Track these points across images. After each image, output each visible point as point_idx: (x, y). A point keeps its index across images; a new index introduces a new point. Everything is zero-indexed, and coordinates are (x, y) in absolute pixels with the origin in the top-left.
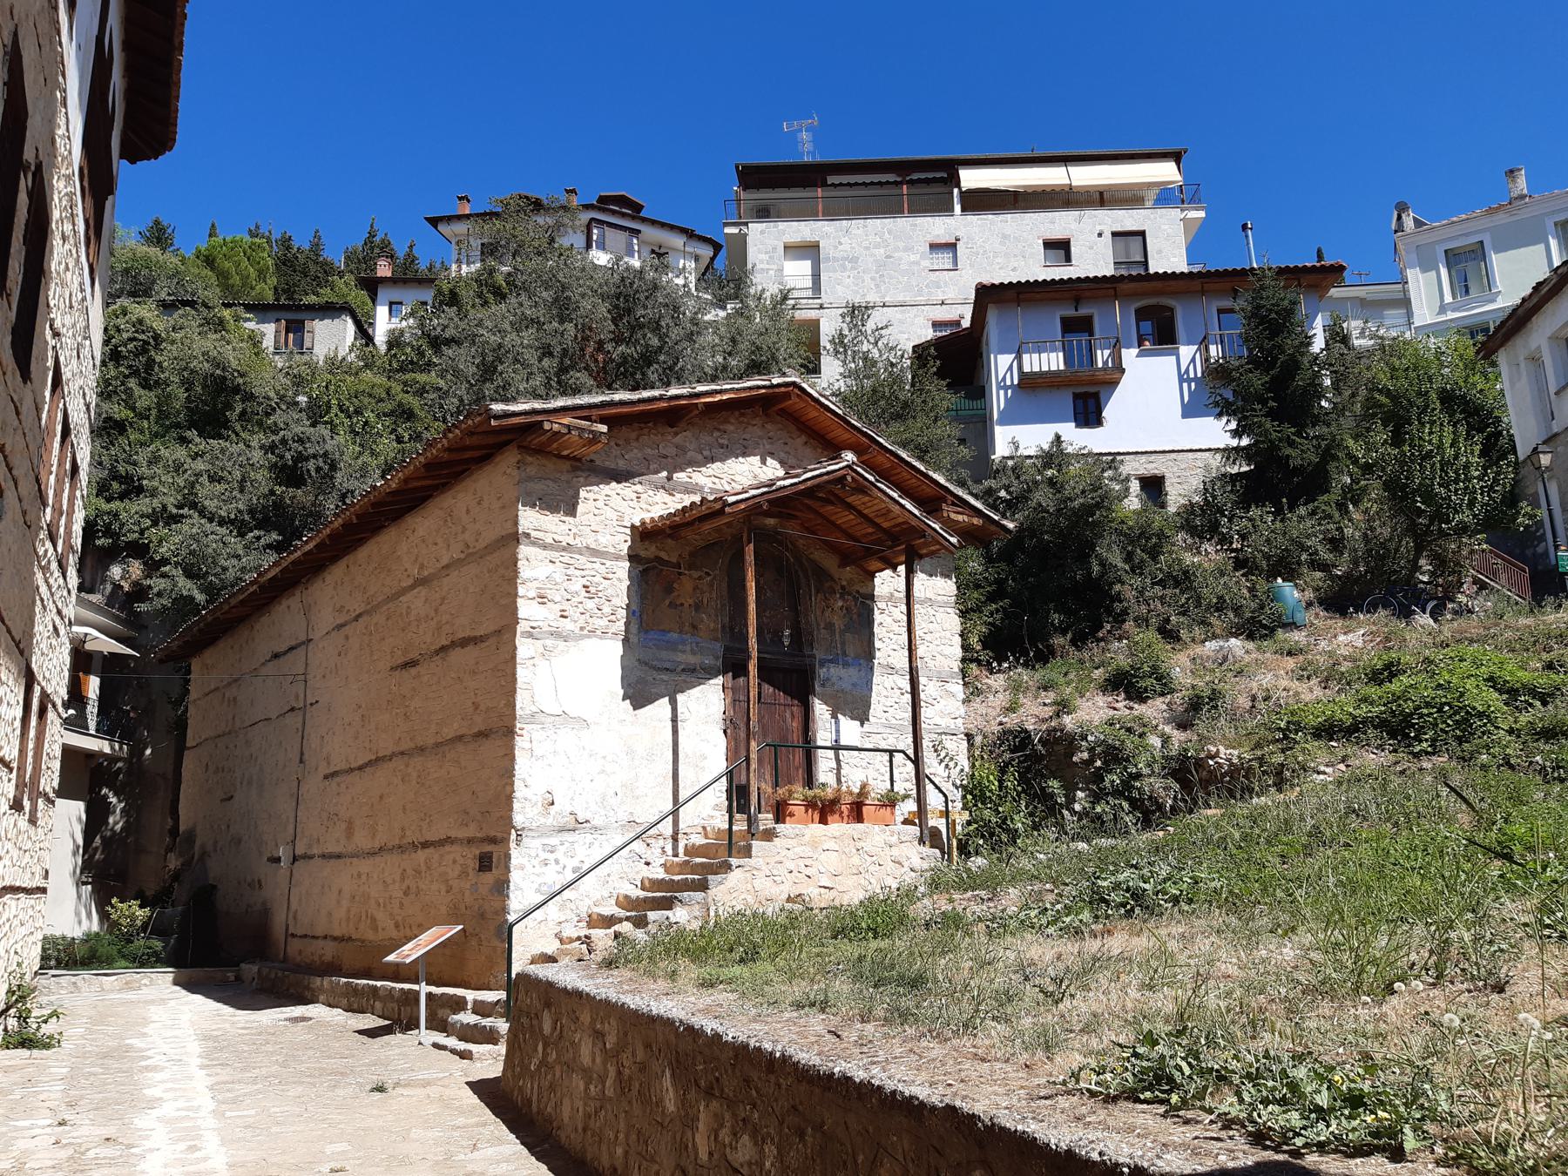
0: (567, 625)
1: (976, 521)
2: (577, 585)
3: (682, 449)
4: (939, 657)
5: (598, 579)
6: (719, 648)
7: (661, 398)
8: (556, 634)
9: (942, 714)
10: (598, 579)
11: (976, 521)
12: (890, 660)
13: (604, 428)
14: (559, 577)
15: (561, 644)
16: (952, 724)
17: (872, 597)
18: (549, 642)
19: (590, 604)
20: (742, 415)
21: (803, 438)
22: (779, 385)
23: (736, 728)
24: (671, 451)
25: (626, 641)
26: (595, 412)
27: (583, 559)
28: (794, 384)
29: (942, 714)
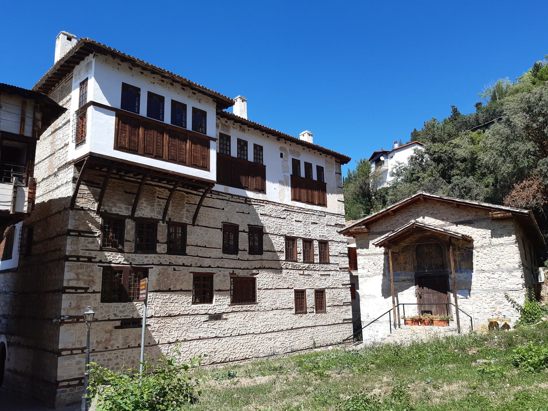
0: (370, 273)
1: (507, 214)
2: (371, 263)
3: (398, 220)
4: (507, 264)
5: (377, 261)
6: (413, 274)
7: (378, 214)
8: (368, 276)
9: (510, 284)
10: (377, 261)
11: (507, 214)
12: (482, 268)
13: (364, 227)
14: (367, 262)
15: (369, 278)
16: (516, 287)
17: (473, 248)
18: (366, 278)
19: (375, 267)
20: (417, 204)
21: (440, 204)
22: (415, 197)
23: (420, 296)
24: (395, 222)
25: (384, 275)
26: (361, 224)
27: (372, 256)
28: (420, 194)
29: (510, 284)
